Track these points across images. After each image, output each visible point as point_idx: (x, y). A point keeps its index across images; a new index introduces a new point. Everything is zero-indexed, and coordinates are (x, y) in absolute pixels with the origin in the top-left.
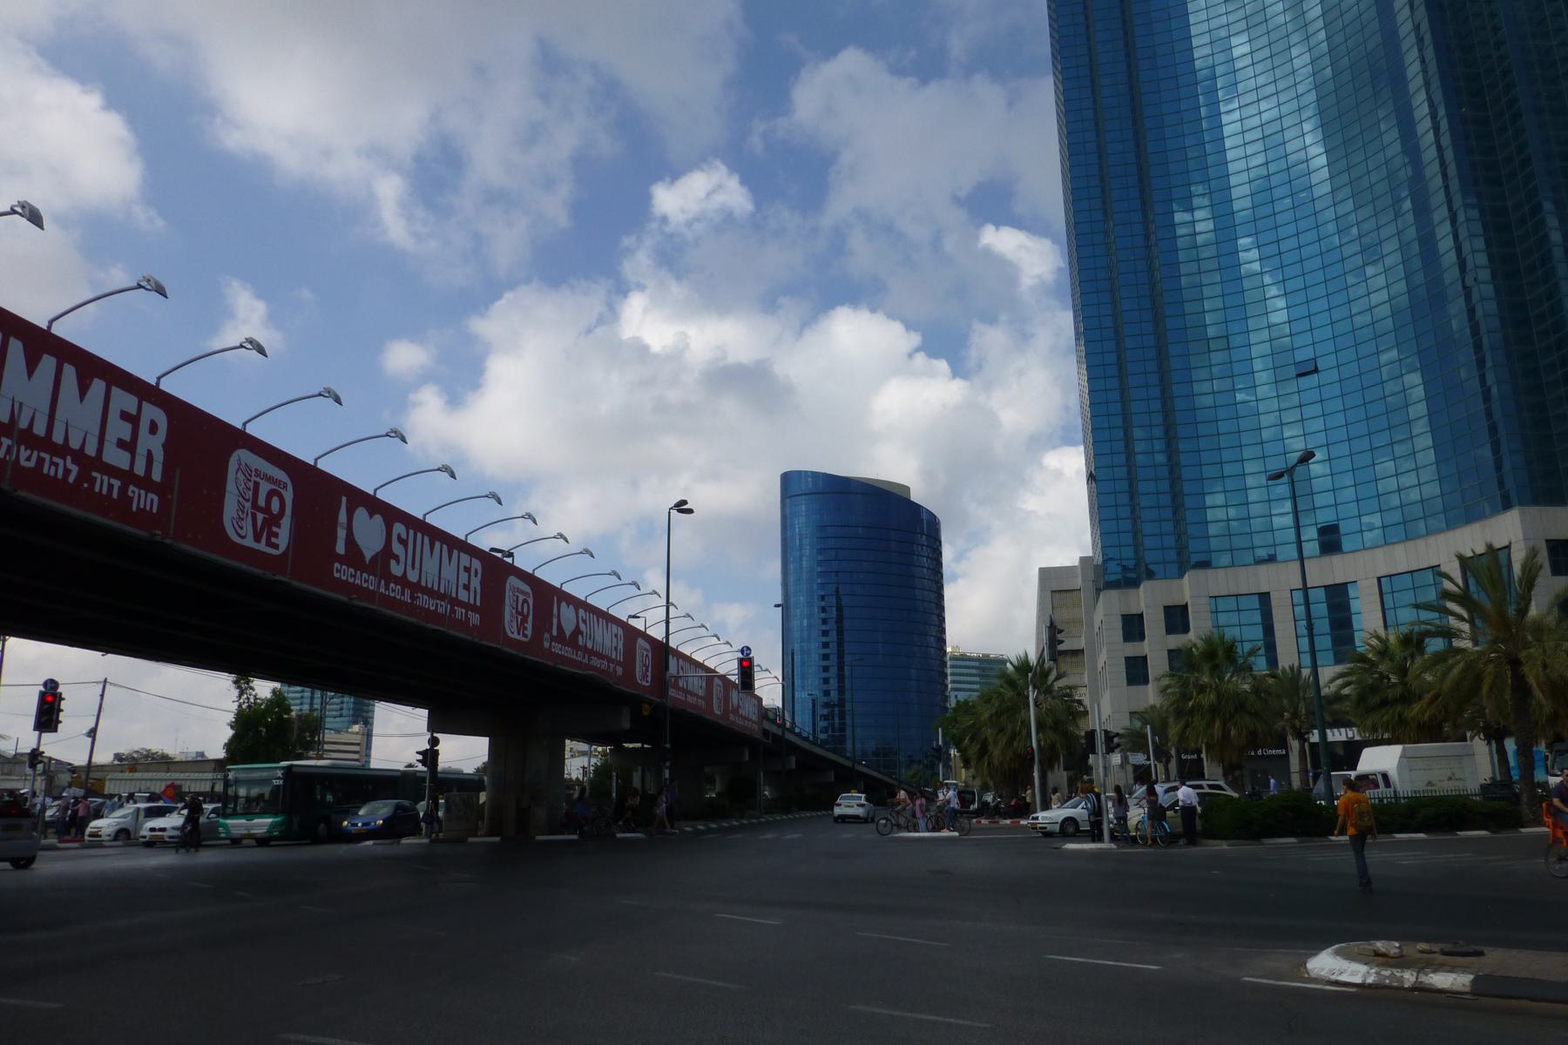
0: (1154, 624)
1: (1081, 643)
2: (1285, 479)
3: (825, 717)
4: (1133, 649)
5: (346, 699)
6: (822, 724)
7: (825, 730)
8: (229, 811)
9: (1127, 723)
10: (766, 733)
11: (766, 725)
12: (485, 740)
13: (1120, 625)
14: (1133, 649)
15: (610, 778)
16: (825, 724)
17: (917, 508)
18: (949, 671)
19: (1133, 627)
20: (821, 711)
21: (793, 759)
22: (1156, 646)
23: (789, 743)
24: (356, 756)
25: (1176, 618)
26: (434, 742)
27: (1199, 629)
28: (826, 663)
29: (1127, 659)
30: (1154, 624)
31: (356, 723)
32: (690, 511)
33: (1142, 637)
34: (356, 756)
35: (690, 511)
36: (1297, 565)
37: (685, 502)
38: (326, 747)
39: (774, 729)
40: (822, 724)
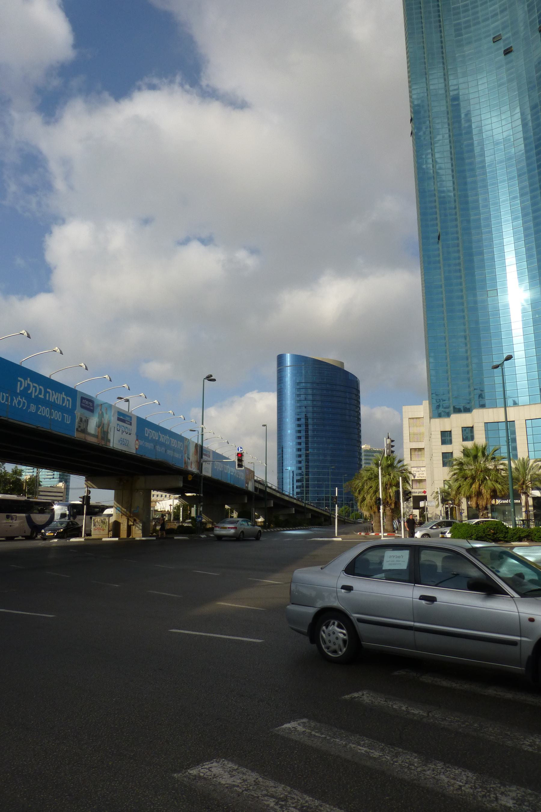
0: (457, 436)
1: (387, 442)
3: (298, 481)
4: (447, 448)
7: (297, 493)
9: (442, 486)
12: (113, 491)
13: (440, 436)
14: (447, 448)
16: (299, 490)
17: (347, 373)
18: (363, 458)
19: (446, 437)
21: (272, 502)
22: (457, 448)
24: (61, 494)
25: (468, 433)
26: (89, 492)
27: (480, 439)
28: (300, 459)
29: (443, 453)
30: (457, 436)
34: (61, 494)
37: (211, 376)
38: (41, 493)
40: (296, 490)
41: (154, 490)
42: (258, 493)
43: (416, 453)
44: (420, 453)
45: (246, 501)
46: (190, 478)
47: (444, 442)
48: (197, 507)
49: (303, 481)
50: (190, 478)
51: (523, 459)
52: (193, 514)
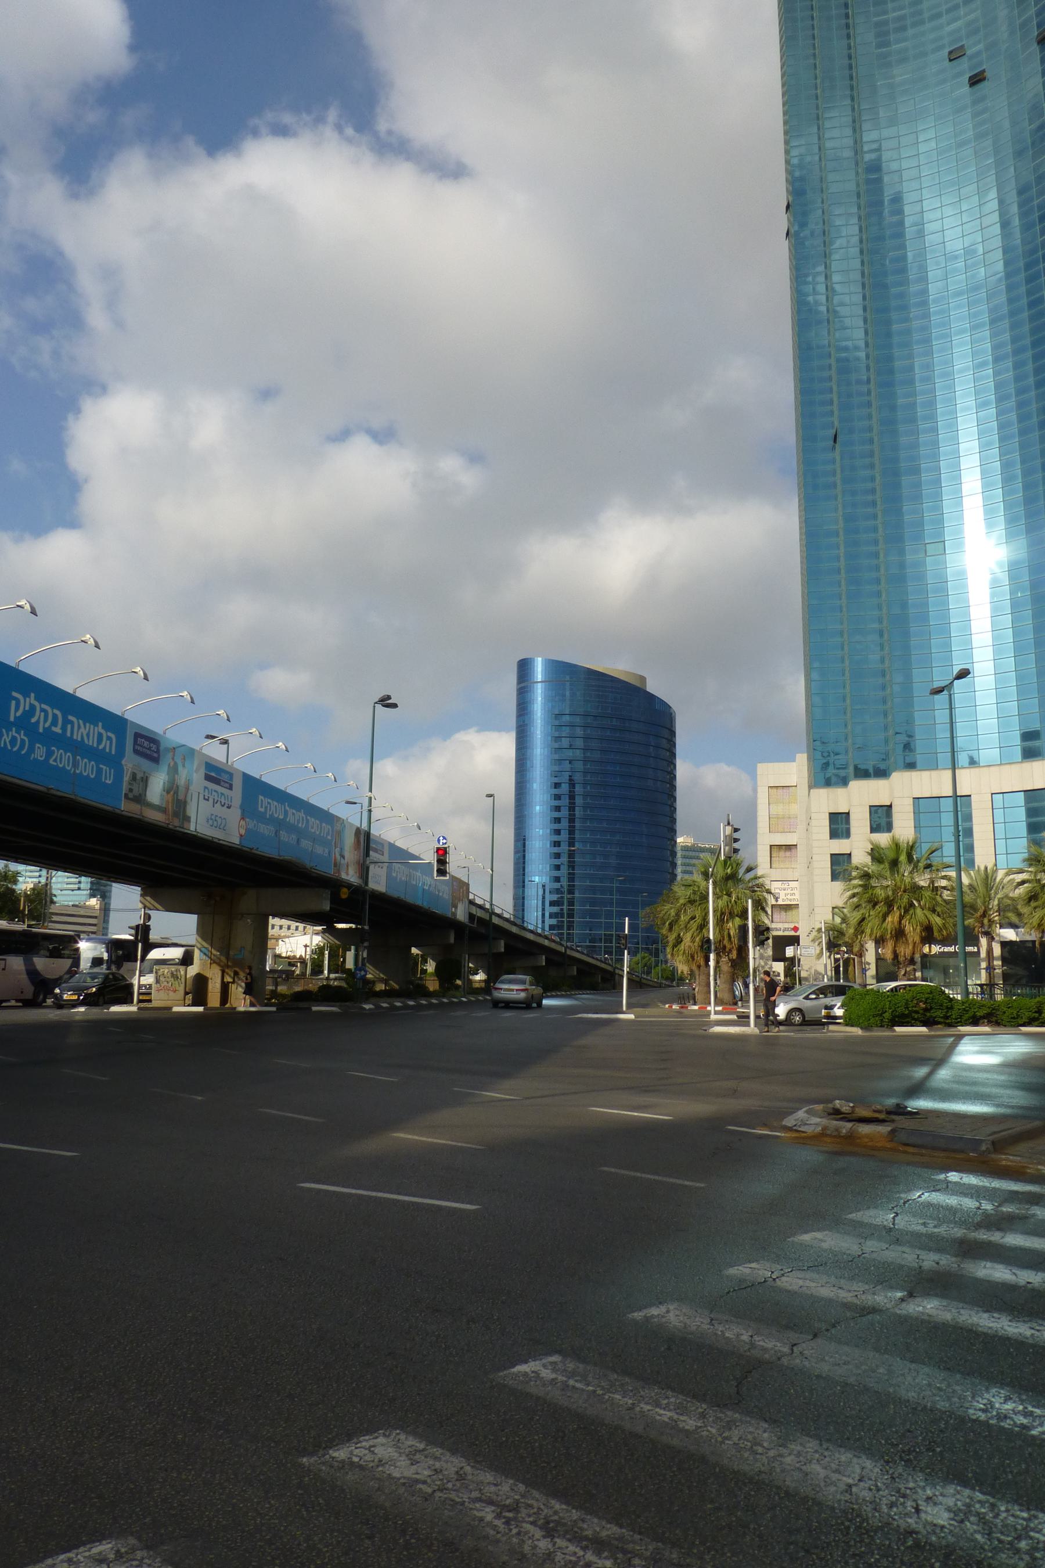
0: (860, 823)
2: (945, 692)
4: (840, 846)
5: (83, 879)
6: (549, 910)
8: (155, 755)
10: (472, 917)
11: (474, 910)
12: (196, 916)
14: (840, 846)
15: (323, 954)
17: (651, 697)
18: (679, 862)
20: (549, 898)
21: (502, 943)
22: (859, 845)
23: (497, 927)
25: (881, 817)
26: (148, 917)
27: (904, 829)
30: (860, 823)
31: (92, 896)
32: (395, 706)
33: (848, 835)
35: (395, 706)
36: (949, 773)
37: (389, 697)
39: (480, 913)
41: (274, 916)
42: (475, 926)
43: (782, 853)
44: (788, 854)
45: (452, 940)
46: (344, 894)
47: (834, 834)
48: (356, 950)
49: (563, 905)
50: (344, 894)
51: (986, 868)
52: (350, 964)
